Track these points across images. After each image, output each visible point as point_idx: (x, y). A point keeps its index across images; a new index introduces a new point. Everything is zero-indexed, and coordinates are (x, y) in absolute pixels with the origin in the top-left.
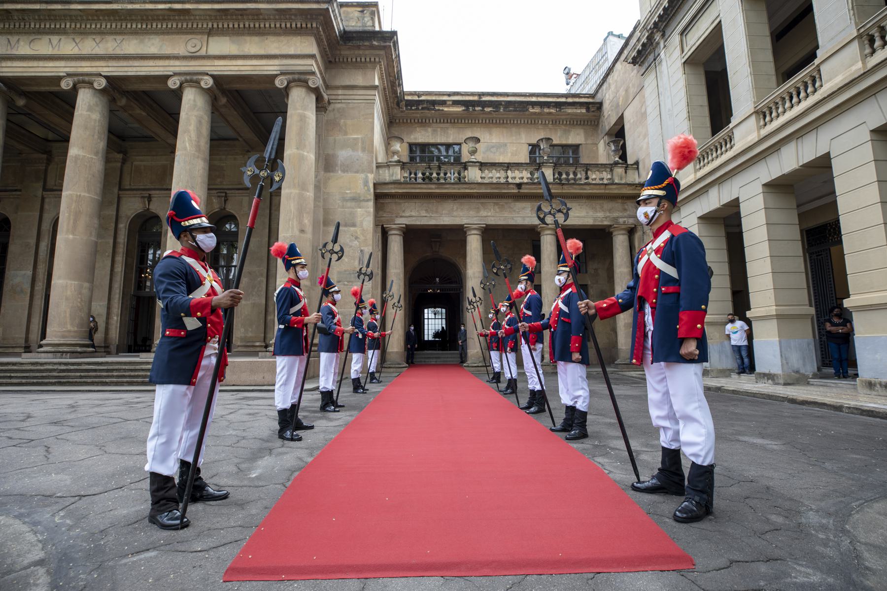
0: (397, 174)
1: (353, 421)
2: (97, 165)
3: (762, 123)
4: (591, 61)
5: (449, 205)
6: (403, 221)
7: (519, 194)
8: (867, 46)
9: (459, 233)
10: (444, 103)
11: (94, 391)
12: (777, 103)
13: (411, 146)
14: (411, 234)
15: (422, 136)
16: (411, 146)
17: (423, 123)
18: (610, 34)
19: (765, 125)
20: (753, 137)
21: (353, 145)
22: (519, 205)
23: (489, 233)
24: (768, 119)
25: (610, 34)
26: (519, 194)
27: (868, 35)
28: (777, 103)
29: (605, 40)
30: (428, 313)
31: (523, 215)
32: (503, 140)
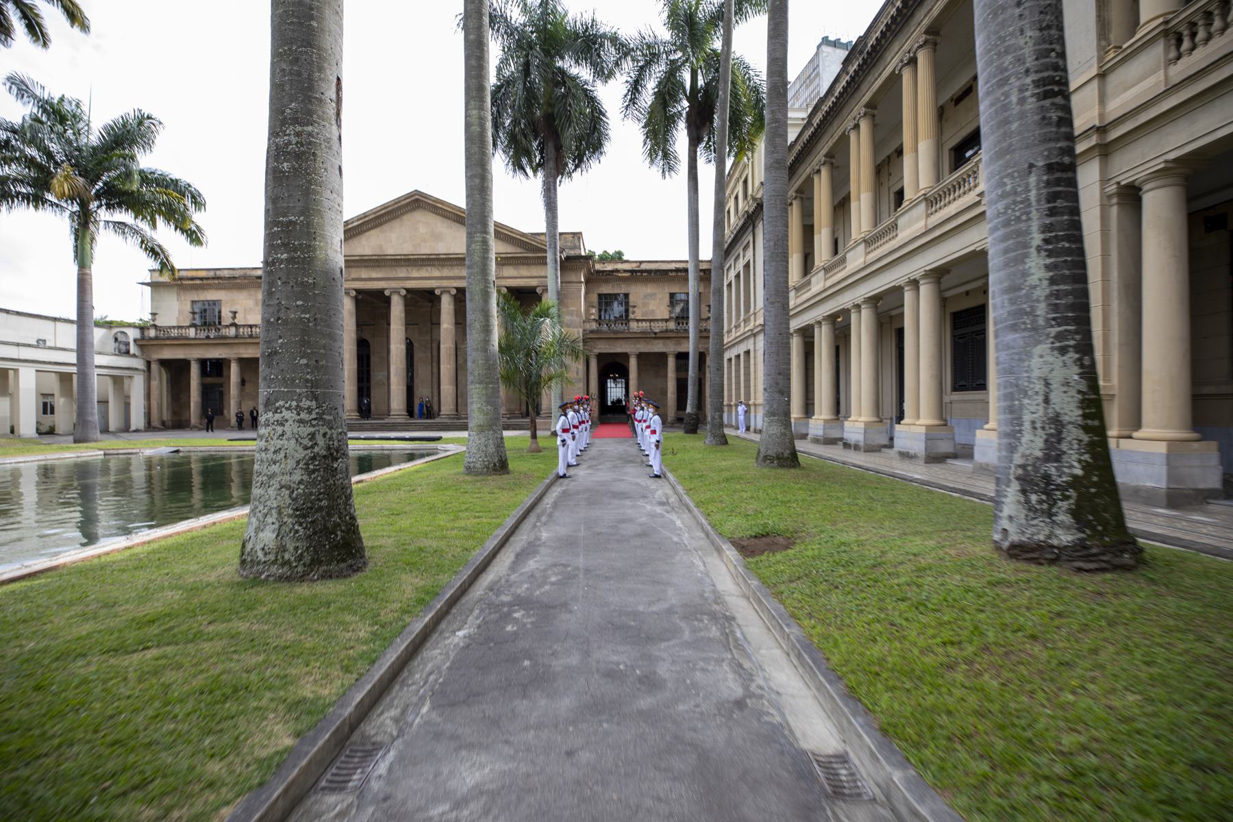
0: (594, 326)
1: (875, 127)
2: (452, 307)
3: (1173, 54)
4: (802, 73)
5: (621, 342)
6: (597, 351)
7: (656, 336)
8: (1173, 48)
9: (626, 356)
10: (617, 271)
11: (50, 363)
12: (1194, 24)
13: (600, 296)
14: (600, 357)
15: (606, 289)
16: (600, 296)
17: (607, 281)
18: (825, 41)
19: (1179, 57)
20: (919, 226)
21: (571, 313)
22: (656, 341)
23: (641, 357)
24: (1186, 44)
25: (825, 41)
26: (656, 336)
27: (1175, 32)
28: (1194, 24)
29: (819, 47)
30: (610, 384)
31: (658, 347)
32: (654, 291)
